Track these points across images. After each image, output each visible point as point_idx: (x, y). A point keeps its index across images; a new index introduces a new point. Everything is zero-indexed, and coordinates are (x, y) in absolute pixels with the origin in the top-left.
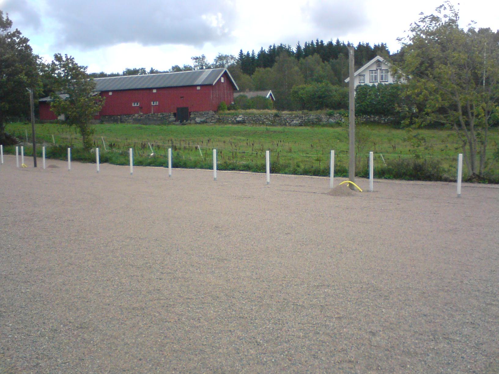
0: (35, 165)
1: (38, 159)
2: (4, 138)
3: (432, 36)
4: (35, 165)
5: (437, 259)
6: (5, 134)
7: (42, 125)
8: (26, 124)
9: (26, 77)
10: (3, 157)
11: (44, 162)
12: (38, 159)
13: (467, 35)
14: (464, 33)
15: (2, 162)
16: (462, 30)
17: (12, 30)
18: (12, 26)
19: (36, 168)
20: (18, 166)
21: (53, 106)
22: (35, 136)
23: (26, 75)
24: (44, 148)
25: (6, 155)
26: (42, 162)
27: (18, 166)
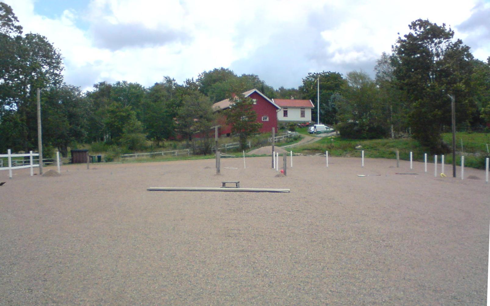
0: (454, 175)
1: (457, 167)
2: (440, 147)
3: (3, 115)
4: (454, 175)
5: (346, 255)
6: (442, 143)
7: (486, 134)
8: (470, 133)
9: (464, 86)
10: (427, 165)
11: (462, 171)
12: (457, 167)
13: (186, 87)
14: (183, 87)
15: (426, 171)
16: (240, 76)
17: (454, 40)
18: (454, 36)
19: (454, 178)
20: (436, 175)
21: (483, 112)
22: (456, 143)
23: (464, 83)
24: (463, 158)
25: (429, 163)
26: (460, 170)
27: (436, 175)
